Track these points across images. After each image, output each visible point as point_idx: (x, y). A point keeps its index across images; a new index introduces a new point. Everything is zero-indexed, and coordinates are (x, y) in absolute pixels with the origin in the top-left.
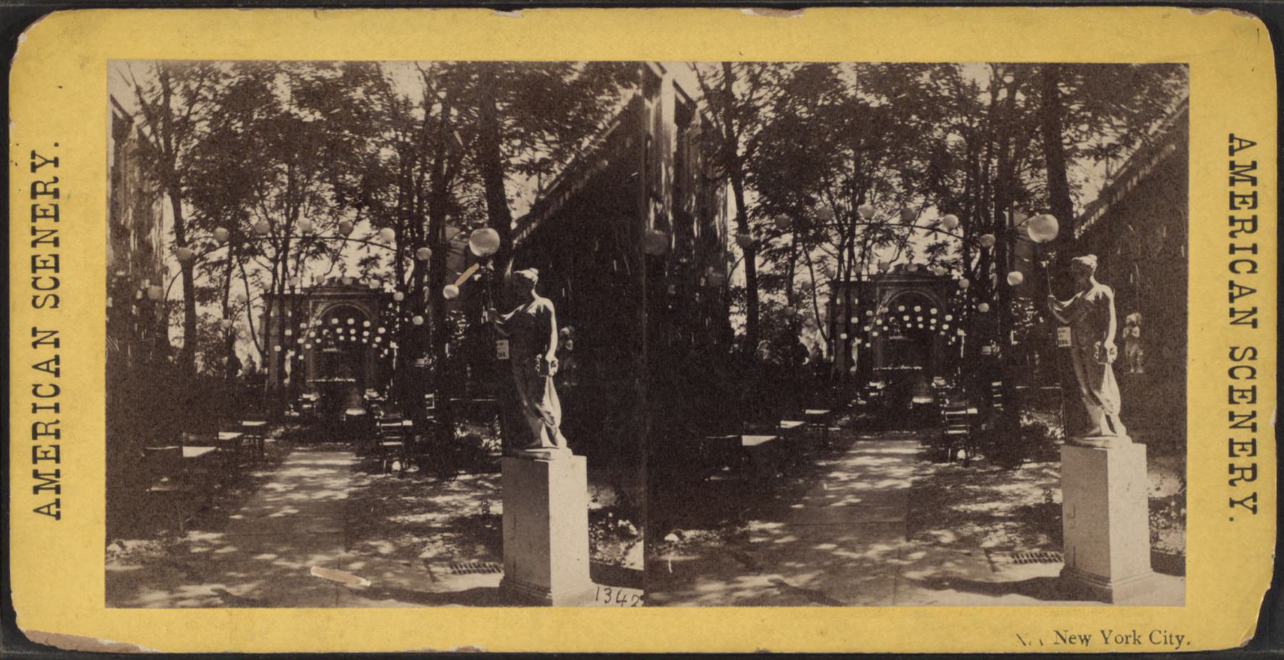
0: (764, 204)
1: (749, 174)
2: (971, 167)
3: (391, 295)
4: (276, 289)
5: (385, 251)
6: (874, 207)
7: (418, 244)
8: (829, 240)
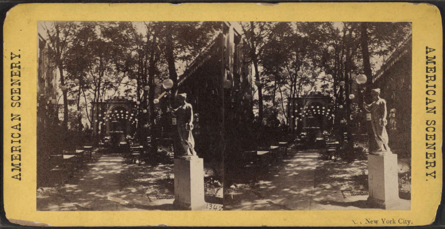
0: (265, 71)
1: (260, 61)
2: (337, 58)
3: (136, 102)
4: (96, 100)
5: (133, 87)
6: (303, 72)
7: (145, 85)
8: (287, 83)
